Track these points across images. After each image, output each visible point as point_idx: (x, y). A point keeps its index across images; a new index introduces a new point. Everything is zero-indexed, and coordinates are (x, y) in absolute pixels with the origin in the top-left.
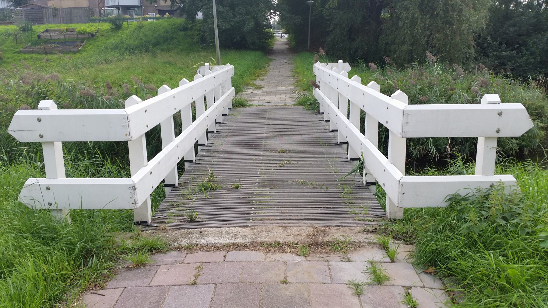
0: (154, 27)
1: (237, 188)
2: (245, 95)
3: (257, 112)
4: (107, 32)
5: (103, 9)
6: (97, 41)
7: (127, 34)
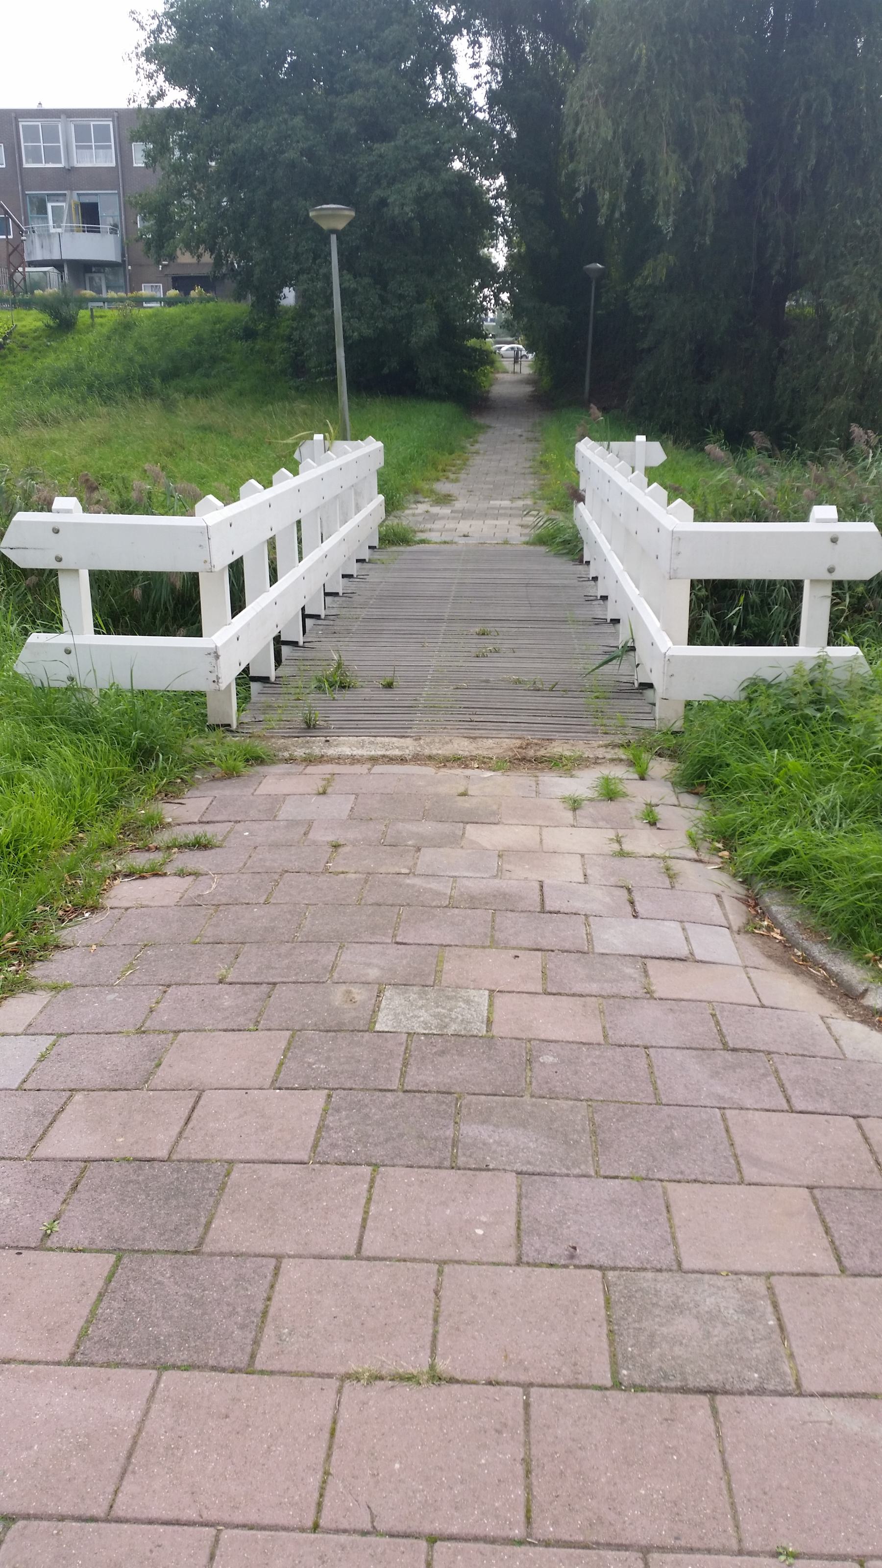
0: (164, 327)
1: (389, 686)
2: (410, 518)
3: (438, 558)
4: (35, 339)
5: (20, 269)
6: (9, 362)
7: (90, 344)
